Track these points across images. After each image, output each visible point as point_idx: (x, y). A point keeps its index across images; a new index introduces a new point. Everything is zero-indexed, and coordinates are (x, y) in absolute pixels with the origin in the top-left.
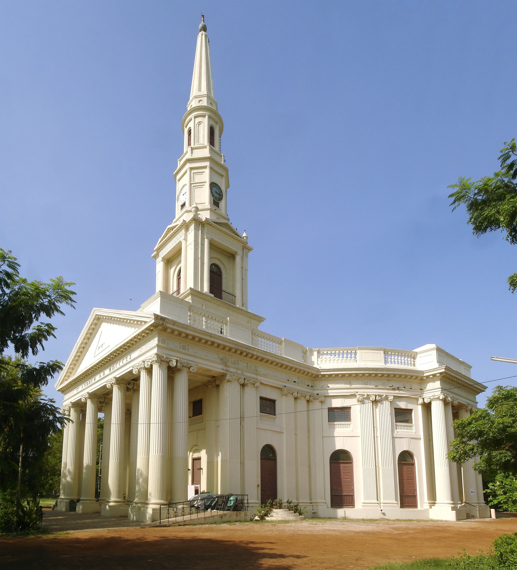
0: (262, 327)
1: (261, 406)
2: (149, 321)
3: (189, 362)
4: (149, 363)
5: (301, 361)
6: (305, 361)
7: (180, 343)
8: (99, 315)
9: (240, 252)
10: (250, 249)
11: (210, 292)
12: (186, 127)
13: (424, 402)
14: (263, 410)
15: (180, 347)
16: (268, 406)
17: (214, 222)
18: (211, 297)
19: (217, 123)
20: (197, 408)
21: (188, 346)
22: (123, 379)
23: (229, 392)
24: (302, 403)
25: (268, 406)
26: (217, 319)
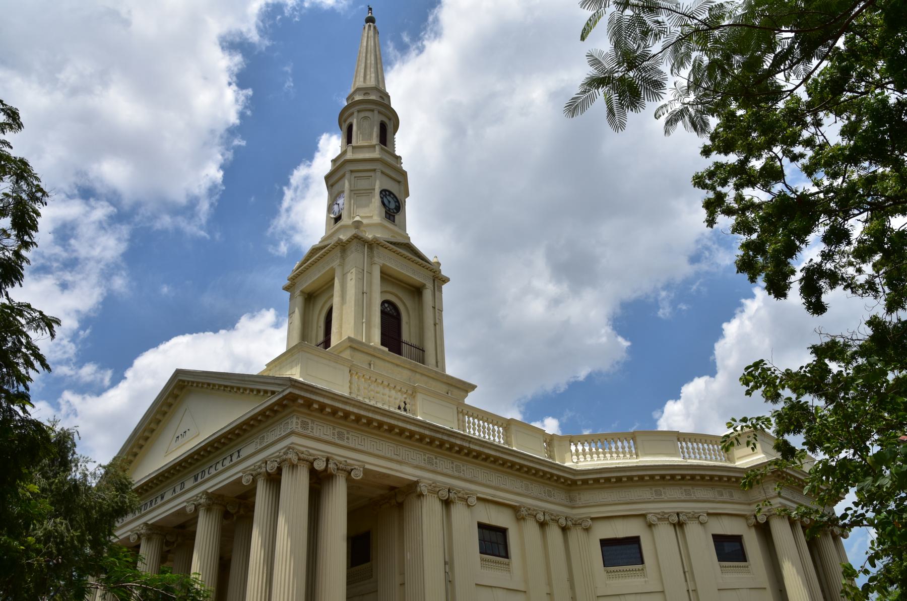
0: (470, 400)
1: (482, 540)
2: (280, 390)
3: (349, 461)
4: (276, 465)
5: (542, 456)
6: (506, 442)
7: (334, 429)
8: (184, 381)
9: (429, 285)
10: (445, 280)
11: (382, 344)
12: (345, 121)
13: (757, 522)
14: (722, 556)
15: (334, 434)
16: (494, 541)
17: (391, 243)
18: (383, 351)
19: (390, 120)
20: (360, 550)
21: (348, 433)
22: (219, 496)
23: (428, 515)
24: (554, 533)
25: (494, 541)
26: (398, 388)
